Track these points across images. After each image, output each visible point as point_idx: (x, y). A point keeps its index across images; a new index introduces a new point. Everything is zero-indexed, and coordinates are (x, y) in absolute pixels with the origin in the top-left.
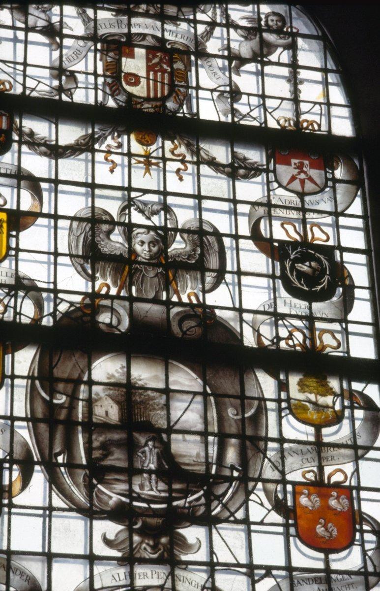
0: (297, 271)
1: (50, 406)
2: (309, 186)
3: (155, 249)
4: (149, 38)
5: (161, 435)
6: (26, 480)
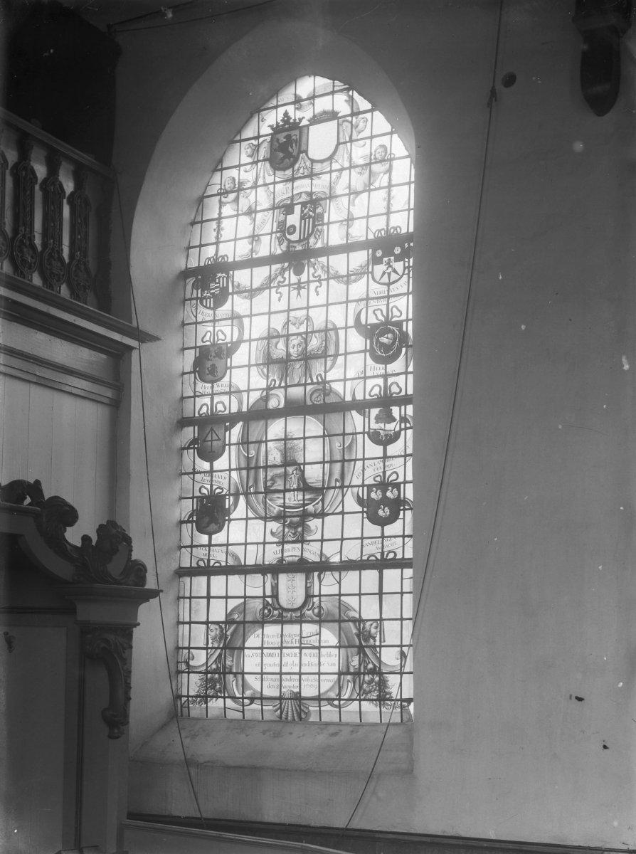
0: (380, 343)
1: (248, 459)
2: (394, 277)
3: (300, 349)
4: (303, 195)
5: (300, 467)
6: (236, 503)
